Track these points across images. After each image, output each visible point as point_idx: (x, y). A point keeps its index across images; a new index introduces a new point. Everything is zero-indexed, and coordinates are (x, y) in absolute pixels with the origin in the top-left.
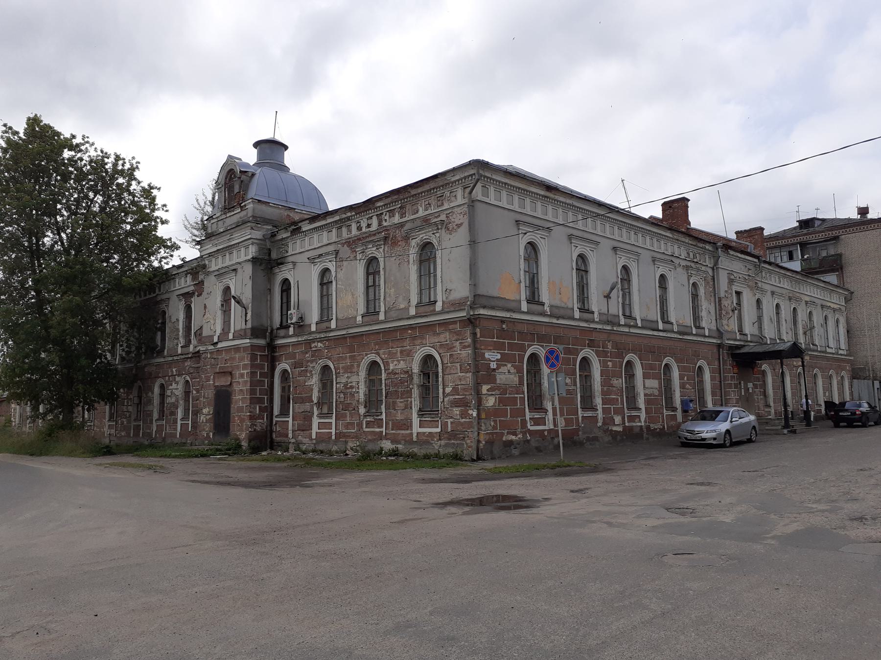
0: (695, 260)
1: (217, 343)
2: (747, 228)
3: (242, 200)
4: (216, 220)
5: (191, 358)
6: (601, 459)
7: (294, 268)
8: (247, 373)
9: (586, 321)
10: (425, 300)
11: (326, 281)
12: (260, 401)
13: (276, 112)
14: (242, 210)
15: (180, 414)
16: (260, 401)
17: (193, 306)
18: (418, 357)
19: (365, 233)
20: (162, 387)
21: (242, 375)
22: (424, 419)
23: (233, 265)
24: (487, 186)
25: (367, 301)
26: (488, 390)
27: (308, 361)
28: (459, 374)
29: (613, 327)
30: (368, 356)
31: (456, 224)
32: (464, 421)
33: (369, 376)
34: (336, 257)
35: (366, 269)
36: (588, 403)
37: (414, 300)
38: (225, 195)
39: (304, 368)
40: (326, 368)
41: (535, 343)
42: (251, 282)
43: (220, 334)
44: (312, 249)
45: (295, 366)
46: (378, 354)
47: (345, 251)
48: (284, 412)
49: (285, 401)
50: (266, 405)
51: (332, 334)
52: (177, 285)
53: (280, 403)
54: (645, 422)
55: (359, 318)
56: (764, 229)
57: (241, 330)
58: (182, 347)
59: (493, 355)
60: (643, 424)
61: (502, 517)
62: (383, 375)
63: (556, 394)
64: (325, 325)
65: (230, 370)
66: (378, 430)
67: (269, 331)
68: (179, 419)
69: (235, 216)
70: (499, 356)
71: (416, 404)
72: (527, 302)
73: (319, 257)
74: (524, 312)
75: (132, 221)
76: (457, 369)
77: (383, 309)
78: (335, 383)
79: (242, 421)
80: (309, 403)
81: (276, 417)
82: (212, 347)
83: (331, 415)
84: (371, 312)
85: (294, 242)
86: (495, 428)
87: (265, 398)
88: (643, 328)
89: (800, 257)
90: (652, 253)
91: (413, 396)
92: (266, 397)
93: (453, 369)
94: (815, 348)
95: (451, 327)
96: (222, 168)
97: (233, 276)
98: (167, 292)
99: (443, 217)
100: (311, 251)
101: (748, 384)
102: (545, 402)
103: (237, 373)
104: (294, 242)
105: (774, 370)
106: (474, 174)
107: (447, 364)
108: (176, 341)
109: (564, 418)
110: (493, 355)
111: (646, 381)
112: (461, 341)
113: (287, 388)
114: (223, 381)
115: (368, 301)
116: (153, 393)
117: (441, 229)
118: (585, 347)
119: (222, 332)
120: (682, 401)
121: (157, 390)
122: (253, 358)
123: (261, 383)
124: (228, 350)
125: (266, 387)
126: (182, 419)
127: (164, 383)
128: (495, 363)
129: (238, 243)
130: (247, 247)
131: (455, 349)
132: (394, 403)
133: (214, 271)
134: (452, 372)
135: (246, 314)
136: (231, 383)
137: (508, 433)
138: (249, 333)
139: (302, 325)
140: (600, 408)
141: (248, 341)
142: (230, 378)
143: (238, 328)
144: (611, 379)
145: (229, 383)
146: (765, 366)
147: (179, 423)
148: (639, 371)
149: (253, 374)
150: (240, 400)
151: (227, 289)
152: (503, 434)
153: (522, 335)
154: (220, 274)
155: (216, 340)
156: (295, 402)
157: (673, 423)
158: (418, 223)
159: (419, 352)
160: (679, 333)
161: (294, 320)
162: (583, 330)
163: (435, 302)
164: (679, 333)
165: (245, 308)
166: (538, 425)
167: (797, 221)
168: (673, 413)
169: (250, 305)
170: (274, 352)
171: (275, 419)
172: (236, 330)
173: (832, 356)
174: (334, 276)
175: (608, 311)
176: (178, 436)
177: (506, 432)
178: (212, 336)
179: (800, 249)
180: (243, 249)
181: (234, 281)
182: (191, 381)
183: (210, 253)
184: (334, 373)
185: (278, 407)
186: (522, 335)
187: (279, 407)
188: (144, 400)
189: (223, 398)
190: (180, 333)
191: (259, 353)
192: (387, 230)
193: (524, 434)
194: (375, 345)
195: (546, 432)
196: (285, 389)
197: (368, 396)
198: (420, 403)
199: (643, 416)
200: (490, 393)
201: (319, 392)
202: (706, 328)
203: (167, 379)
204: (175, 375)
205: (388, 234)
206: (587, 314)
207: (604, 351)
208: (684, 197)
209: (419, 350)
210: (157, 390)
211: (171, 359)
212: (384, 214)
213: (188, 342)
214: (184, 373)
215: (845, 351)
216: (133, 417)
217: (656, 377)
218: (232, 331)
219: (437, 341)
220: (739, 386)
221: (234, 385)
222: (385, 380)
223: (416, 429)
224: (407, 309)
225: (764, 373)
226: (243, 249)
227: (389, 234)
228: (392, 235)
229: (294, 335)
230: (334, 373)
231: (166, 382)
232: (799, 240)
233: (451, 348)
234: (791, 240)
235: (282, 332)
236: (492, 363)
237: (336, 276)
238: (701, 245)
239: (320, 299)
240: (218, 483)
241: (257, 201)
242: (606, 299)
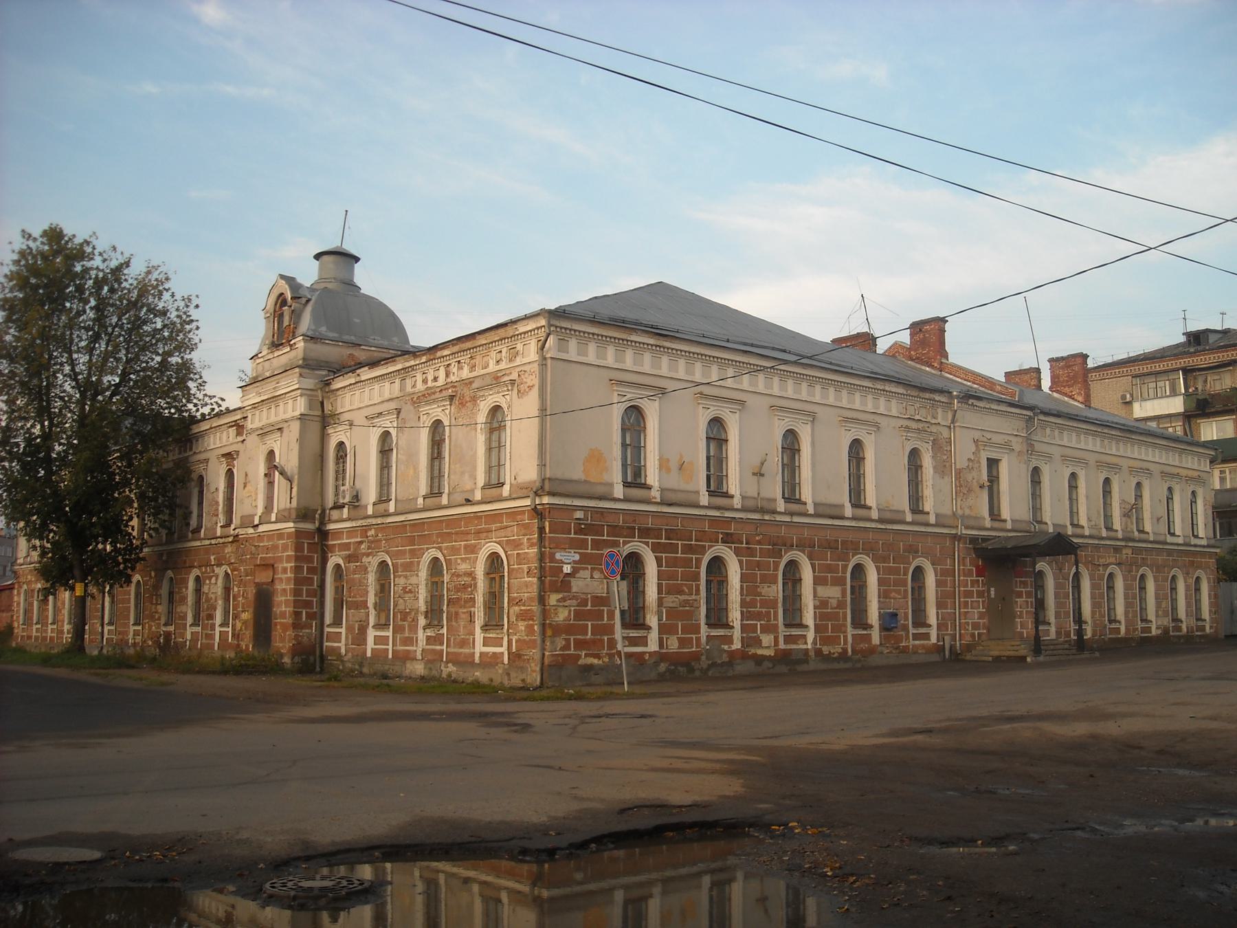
0: (917, 417)
1: (257, 526)
2: (1065, 354)
3: (293, 336)
4: (262, 360)
5: (232, 542)
7: (350, 429)
8: (291, 567)
9: (718, 508)
10: (494, 481)
11: (387, 449)
12: (308, 604)
13: (347, 211)
14: (291, 350)
15: (218, 619)
16: (308, 604)
17: (235, 471)
18: (483, 555)
19: (431, 388)
20: (198, 579)
21: (285, 570)
22: (489, 636)
23: (279, 422)
24: (566, 339)
25: (431, 478)
26: (558, 601)
27: (364, 554)
28: (526, 579)
29: (763, 515)
30: (429, 551)
31: (528, 385)
33: (431, 577)
34: (398, 418)
35: (431, 432)
36: (718, 617)
37: (481, 481)
38: (274, 326)
39: (358, 564)
40: (383, 564)
41: (636, 539)
42: (298, 447)
43: (263, 513)
44: (371, 405)
45: (349, 559)
46: (440, 549)
47: (408, 409)
48: (337, 622)
49: (339, 604)
50: (315, 610)
51: (390, 520)
52: (218, 442)
53: (333, 609)
54: (814, 643)
55: (420, 501)
57: (285, 510)
58: (221, 527)
59: (568, 556)
60: (809, 646)
62: (445, 577)
63: (618, 608)
64: (382, 507)
65: (272, 562)
66: (438, 648)
67: (319, 512)
68: (217, 625)
69: (285, 356)
70: (577, 557)
71: (480, 618)
72: (623, 486)
73: (377, 417)
74: (619, 500)
76: (523, 572)
77: (446, 491)
78: (392, 585)
79: (285, 630)
80: (364, 609)
81: (328, 626)
82: (251, 531)
83: (387, 627)
84: (435, 492)
85: (352, 393)
86: (567, 647)
87: (313, 601)
88: (816, 515)
89: (1183, 391)
90: (839, 410)
91: (476, 606)
92: (315, 600)
93: (520, 573)
94: (1143, 536)
95: (519, 517)
97: (278, 437)
98: (206, 451)
99: (514, 376)
100: (371, 407)
102: (648, 617)
103: (280, 566)
104: (352, 393)
105: (1060, 570)
106: (544, 326)
107: (514, 565)
108: (215, 518)
109: (677, 638)
110: (568, 556)
111: (819, 588)
112: (528, 536)
113: (340, 588)
114: (263, 577)
115: (432, 479)
116: (187, 588)
117: (512, 390)
118: (718, 543)
119: (265, 510)
120: (881, 616)
121: (191, 584)
122: (298, 548)
123: (309, 581)
124: (270, 535)
125: (315, 587)
126: (221, 626)
127: (200, 575)
128: (569, 566)
129: (286, 393)
130: (295, 399)
131: (522, 547)
132: (457, 613)
133: (257, 429)
134: (519, 576)
135: (291, 488)
136: (272, 581)
137: (586, 655)
138: (294, 515)
139: (358, 506)
140: (737, 624)
141: (291, 525)
142: (272, 574)
143: (282, 506)
144: (759, 586)
145: (270, 580)
146: (1042, 565)
147: (218, 629)
148: (807, 575)
149: (297, 569)
150: (283, 605)
151: (271, 454)
152: (579, 657)
153: (615, 530)
154: (264, 433)
155: (256, 522)
156: (348, 608)
157: (864, 646)
158: (488, 380)
159: (484, 548)
160: (880, 521)
161: (347, 500)
162: (714, 521)
163: (503, 484)
164: (880, 521)
165: (290, 481)
166: (636, 645)
167: (1183, 334)
168: (865, 632)
169: (296, 477)
170: (327, 540)
171: (327, 630)
172: (279, 509)
173: (1161, 547)
174: (394, 443)
175: (759, 494)
176: (216, 648)
177: (583, 653)
178: (253, 516)
179: (1183, 378)
180: (290, 402)
181: (278, 442)
182: (232, 574)
183: (253, 404)
184: (392, 571)
185: (330, 614)
186: (615, 530)
187: (332, 614)
188: (177, 597)
189: (263, 601)
190: (220, 508)
191: (305, 541)
192: (455, 387)
193: (611, 656)
194: (437, 537)
195: (647, 654)
196: (339, 590)
197: (429, 604)
198: (485, 614)
199: (811, 636)
200: (561, 604)
201: (376, 595)
202: (932, 512)
203: (204, 570)
204: (214, 565)
205: (456, 392)
206: (724, 499)
207: (748, 548)
209: (484, 546)
210: (191, 584)
211: (207, 542)
212: (453, 366)
213: (228, 524)
214: (223, 562)
215: (1205, 539)
216: (163, 621)
217: (840, 582)
218: (275, 510)
219: (503, 535)
220: (986, 594)
221: (276, 582)
222: (447, 583)
223: (479, 648)
224: (472, 491)
225: (1041, 574)
226: (290, 402)
227: (456, 392)
228: (459, 393)
229: (349, 519)
230: (392, 571)
231: (202, 573)
232: (1182, 363)
233: (518, 545)
234: (1223, 356)
235: (335, 514)
236: (565, 566)
237: (397, 443)
238: (927, 395)
239: (379, 472)
240: (694, 745)
241: (309, 338)
242: (7, 280)
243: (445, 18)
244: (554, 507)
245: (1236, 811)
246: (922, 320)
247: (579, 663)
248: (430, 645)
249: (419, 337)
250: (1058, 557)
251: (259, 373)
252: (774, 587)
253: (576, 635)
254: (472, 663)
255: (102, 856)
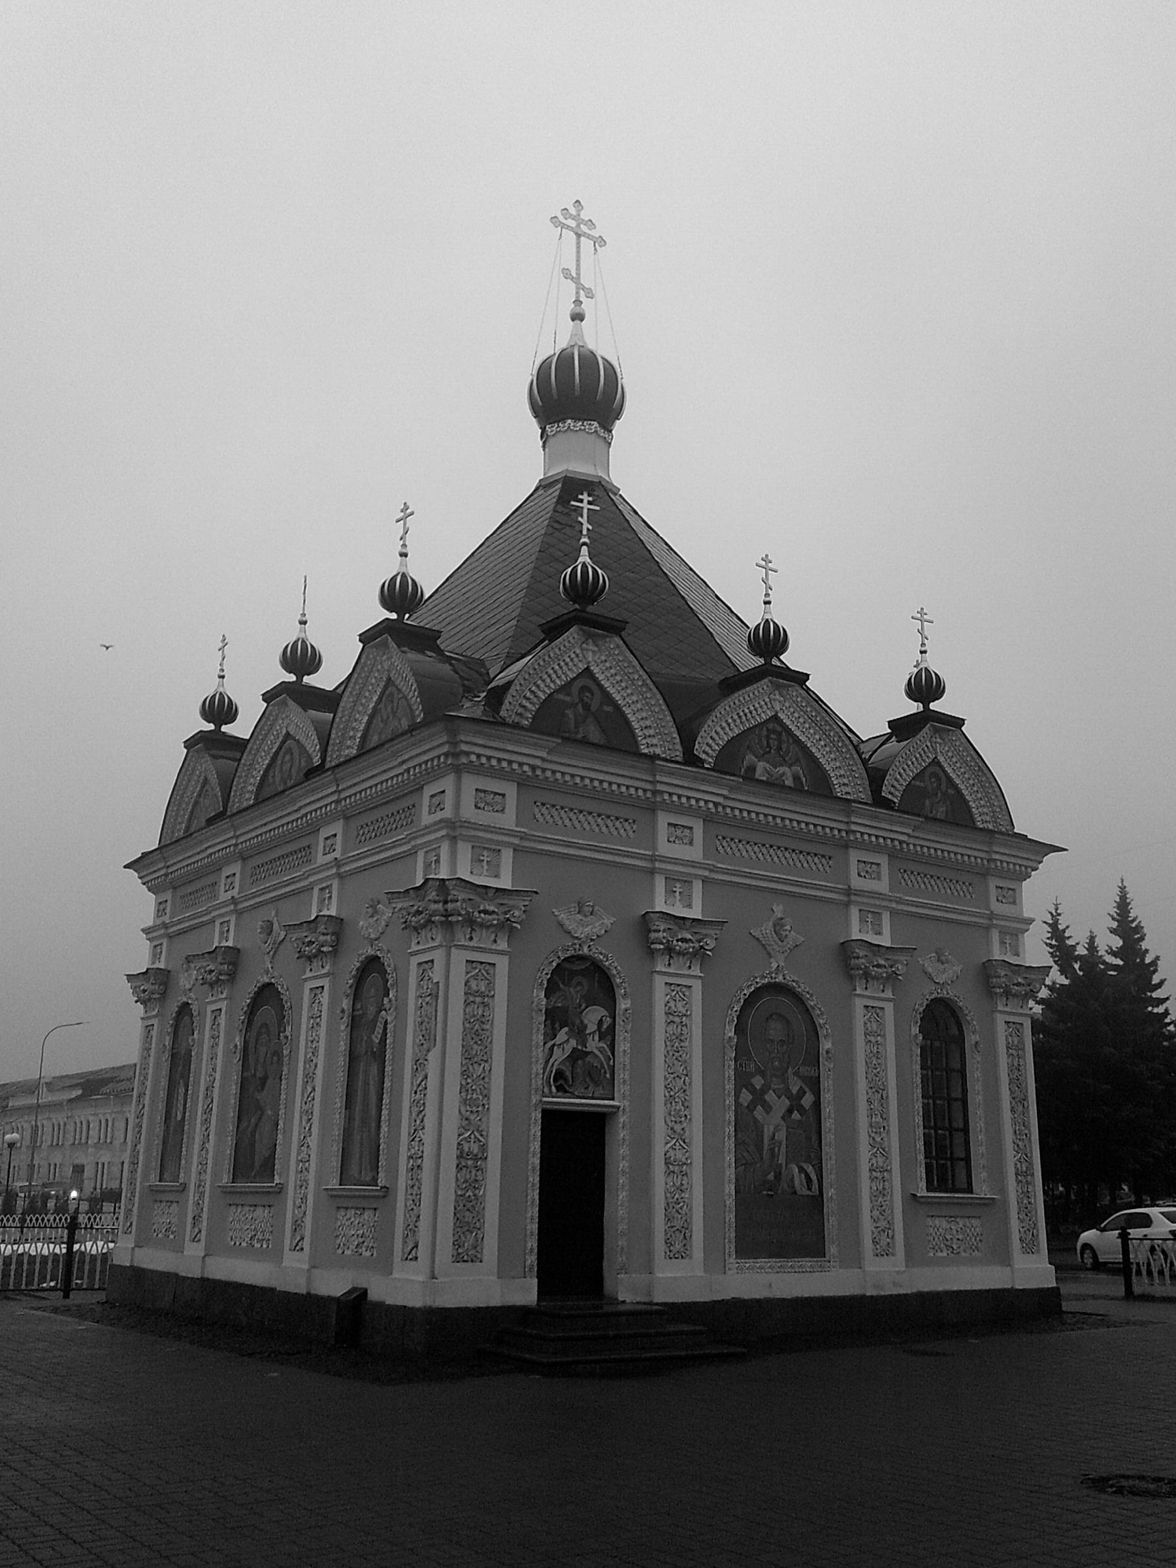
6: (764, 791)
32: (1132, 1269)
56: (619, 490)
61: (637, 510)
75: (1149, 1199)
96: (144, 855)
101: (526, 1292)
208: (1148, 1215)
243: (578, 252)
244: (367, 1194)
245: (1175, 1204)
246: (467, 1308)
247: (1153, 983)
248: (588, 512)
249: (864, 739)
250: (904, 1265)
251: (1065, 1316)
252: (514, 825)
253: (1132, 1272)
254: (709, 820)
255: (450, 819)
